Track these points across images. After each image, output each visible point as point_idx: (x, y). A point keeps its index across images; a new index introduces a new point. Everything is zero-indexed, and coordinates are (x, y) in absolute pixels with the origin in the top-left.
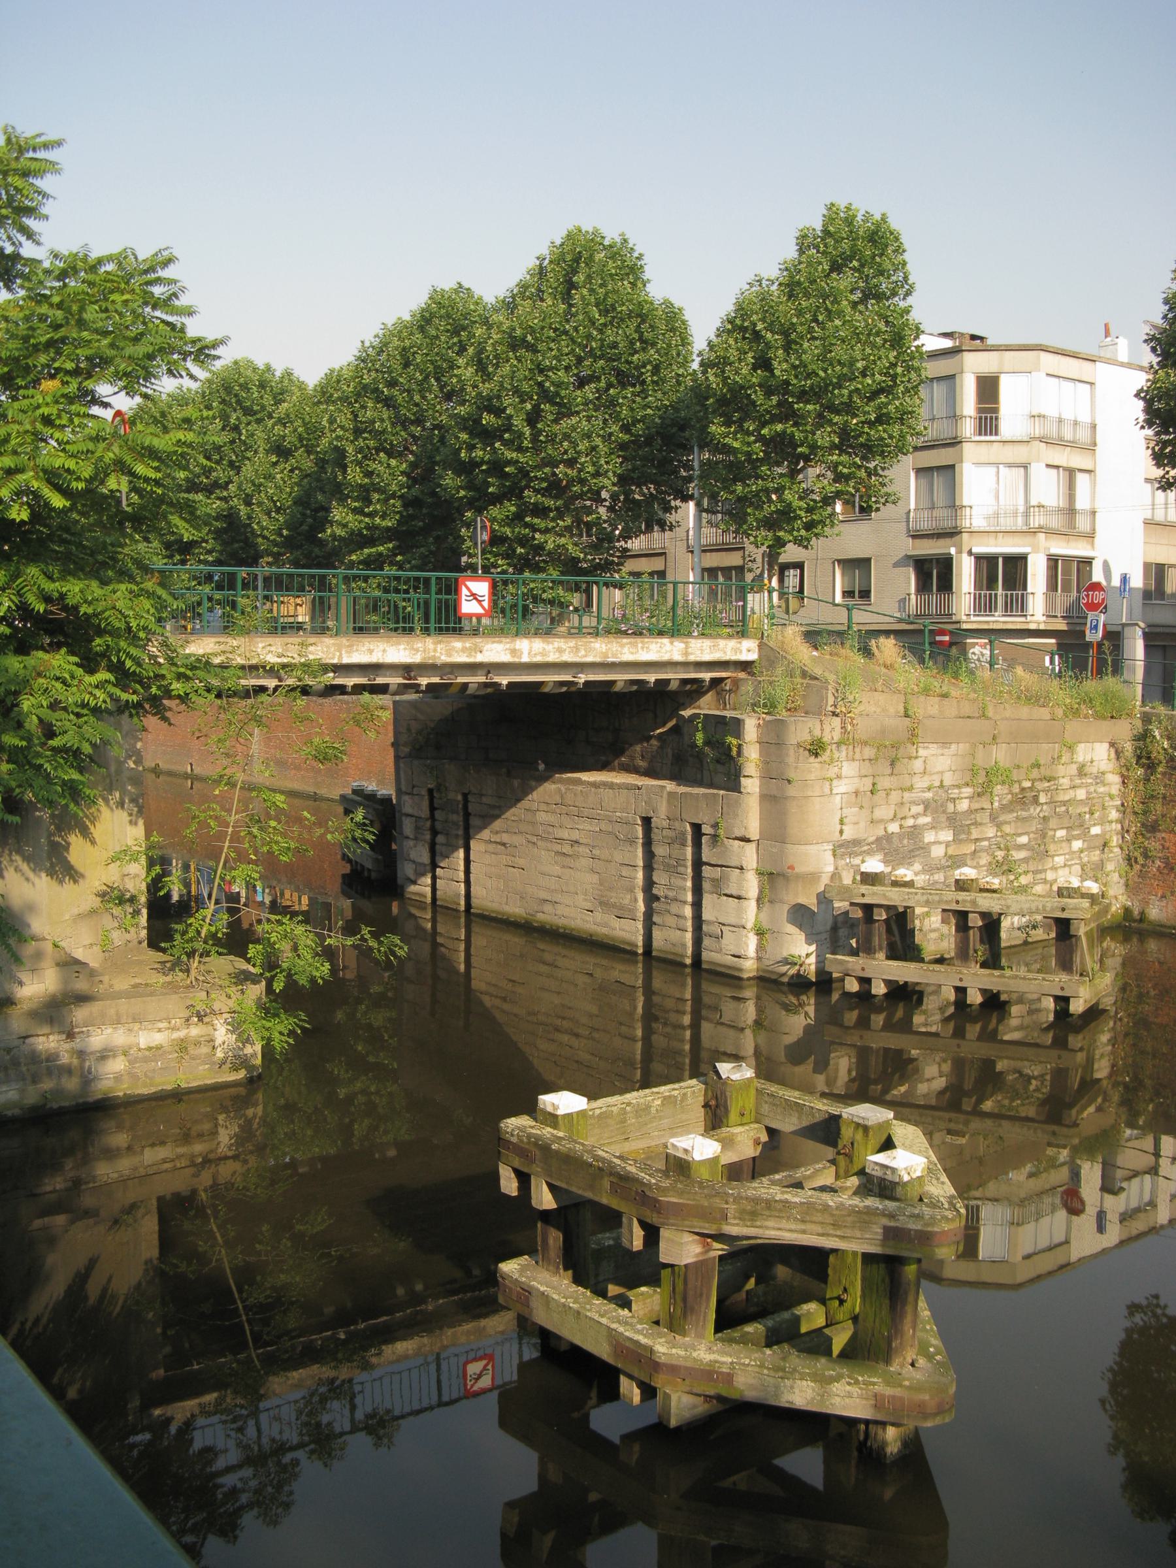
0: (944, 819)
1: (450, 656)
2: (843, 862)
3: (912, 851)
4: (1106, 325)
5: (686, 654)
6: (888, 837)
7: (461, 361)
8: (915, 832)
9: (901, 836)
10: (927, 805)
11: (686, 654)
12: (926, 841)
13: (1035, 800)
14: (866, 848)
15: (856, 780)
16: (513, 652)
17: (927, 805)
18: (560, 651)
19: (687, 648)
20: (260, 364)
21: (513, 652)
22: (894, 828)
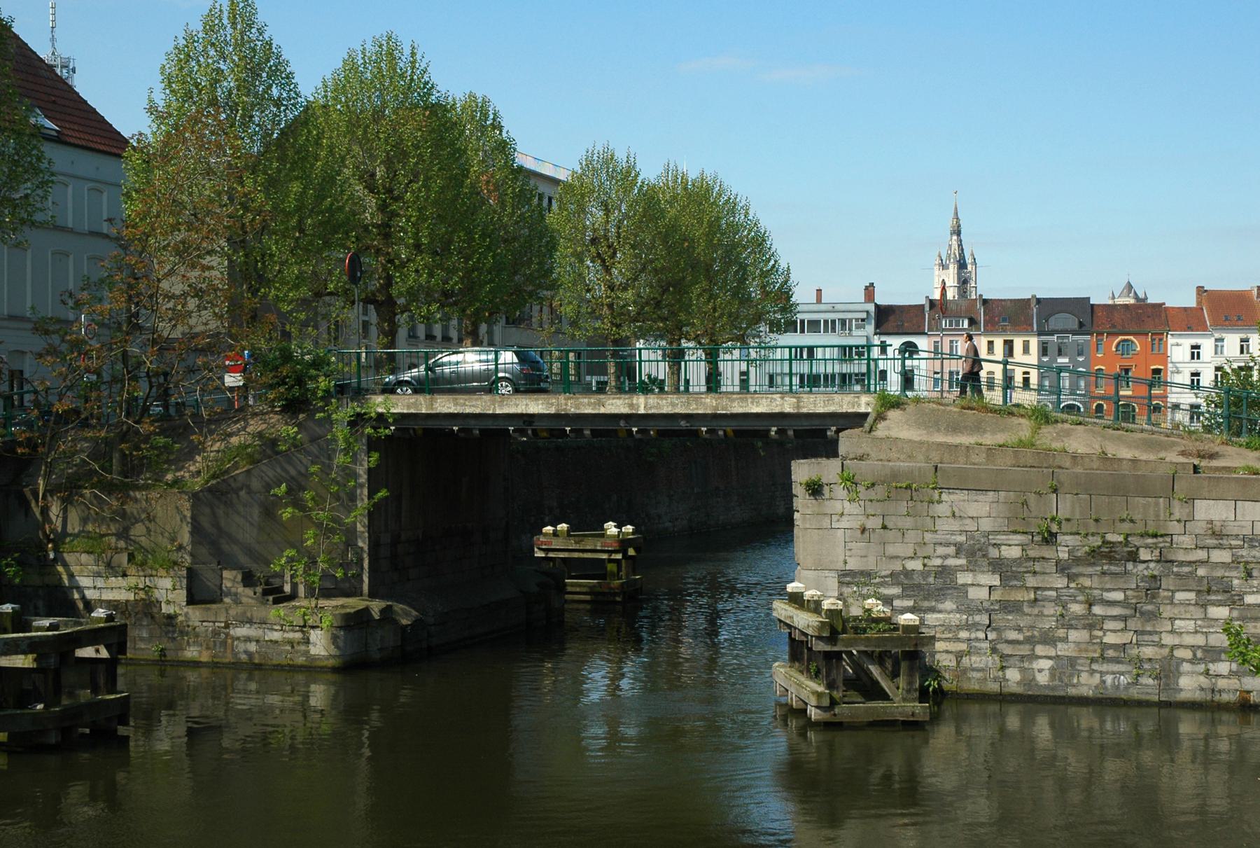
0: (985, 563)
1: (577, 407)
2: (849, 590)
3: (941, 589)
4: (819, 291)
5: (798, 407)
6: (908, 574)
7: (145, 428)
8: (944, 571)
9: (925, 574)
10: (959, 549)
11: (798, 407)
12: (960, 581)
13: (1133, 557)
14: (878, 580)
15: (863, 518)
16: (631, 405)
17: (959, 549)
18: (673, 405)
19: (798, 402)
20: (693, 175)
21: (631, 405)
22: (915, 565)
